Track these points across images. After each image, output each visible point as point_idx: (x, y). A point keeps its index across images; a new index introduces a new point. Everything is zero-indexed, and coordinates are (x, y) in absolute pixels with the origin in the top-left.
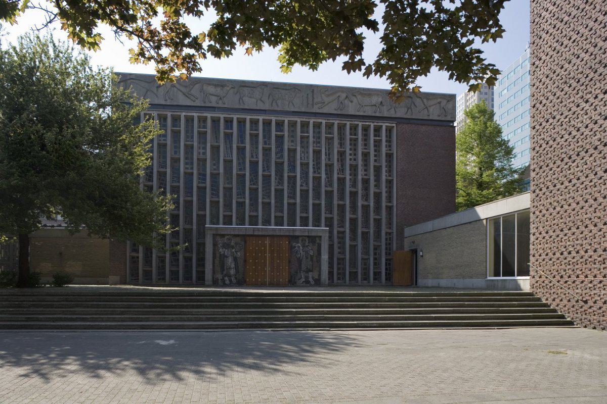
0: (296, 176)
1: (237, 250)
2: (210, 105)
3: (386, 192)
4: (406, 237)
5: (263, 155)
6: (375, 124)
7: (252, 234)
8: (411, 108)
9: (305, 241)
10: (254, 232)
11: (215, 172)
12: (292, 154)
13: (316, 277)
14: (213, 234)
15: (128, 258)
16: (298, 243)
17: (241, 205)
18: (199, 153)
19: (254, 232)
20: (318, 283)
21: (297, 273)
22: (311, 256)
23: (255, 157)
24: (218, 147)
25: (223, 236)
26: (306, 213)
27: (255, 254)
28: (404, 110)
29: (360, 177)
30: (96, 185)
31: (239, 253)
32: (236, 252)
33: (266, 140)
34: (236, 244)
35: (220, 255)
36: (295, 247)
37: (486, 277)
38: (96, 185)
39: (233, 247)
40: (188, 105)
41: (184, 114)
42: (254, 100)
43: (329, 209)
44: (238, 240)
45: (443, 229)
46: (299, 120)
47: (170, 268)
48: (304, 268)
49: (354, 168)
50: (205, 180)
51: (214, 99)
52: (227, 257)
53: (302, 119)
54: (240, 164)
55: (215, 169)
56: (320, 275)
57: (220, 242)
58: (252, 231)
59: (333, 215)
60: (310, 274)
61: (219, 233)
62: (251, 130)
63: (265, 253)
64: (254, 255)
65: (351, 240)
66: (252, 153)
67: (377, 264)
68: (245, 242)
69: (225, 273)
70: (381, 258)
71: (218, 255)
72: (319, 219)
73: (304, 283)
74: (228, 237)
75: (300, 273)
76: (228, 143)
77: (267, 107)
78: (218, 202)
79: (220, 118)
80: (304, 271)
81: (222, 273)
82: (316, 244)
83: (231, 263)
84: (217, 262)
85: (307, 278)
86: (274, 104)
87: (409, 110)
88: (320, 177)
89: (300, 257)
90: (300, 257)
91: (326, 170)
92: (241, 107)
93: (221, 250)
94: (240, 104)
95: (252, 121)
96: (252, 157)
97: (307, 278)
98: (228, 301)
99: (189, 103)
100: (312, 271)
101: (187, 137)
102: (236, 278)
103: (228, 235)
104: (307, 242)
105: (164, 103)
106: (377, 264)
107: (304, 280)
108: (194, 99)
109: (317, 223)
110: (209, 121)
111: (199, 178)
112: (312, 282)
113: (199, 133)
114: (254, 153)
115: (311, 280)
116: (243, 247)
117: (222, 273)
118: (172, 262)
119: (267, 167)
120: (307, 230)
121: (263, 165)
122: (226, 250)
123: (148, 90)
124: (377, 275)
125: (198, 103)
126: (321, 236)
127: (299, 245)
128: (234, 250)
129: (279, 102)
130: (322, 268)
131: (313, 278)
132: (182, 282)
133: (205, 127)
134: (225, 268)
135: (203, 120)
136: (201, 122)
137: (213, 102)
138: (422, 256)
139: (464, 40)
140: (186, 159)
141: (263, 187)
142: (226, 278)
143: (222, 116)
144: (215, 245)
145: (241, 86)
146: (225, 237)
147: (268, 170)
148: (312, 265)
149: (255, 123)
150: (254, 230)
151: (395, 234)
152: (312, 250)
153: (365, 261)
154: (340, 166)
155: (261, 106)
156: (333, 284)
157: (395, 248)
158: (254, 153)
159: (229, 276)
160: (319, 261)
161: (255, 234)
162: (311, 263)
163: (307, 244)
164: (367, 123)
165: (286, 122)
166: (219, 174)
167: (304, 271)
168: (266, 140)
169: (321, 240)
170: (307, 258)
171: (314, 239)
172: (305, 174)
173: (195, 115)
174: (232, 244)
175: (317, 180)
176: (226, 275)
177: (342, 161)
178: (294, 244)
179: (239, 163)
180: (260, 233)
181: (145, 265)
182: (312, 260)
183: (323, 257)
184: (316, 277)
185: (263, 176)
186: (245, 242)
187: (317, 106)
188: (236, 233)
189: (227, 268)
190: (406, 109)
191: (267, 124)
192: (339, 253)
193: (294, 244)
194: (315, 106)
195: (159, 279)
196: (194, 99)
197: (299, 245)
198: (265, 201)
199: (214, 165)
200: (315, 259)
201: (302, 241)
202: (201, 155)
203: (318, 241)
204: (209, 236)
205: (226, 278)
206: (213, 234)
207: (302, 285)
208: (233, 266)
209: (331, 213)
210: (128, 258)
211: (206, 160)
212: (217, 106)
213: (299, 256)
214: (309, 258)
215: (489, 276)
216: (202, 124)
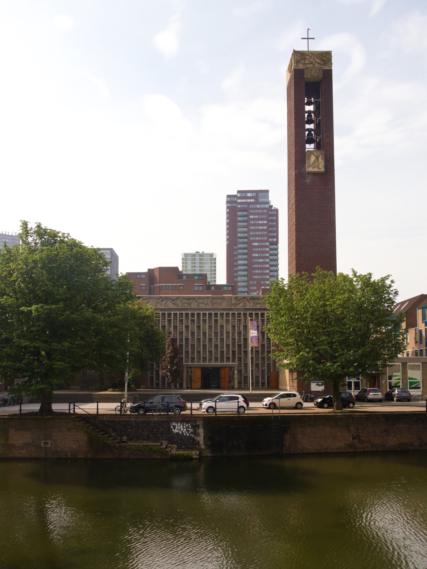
0: (224, 338)
5: (209, 329)
6: (261, 312)
11: (187, 337)
12: (221, 328)
15: (149, 377)
17: (199, 352)
18: (180, 329)
24: (188, 326)
25: (191, 368)
41: (173, 312)
43: (240, 353)
50: (182, 341)
51: (186, 305)
53: (226, 312)
55: (187, 336)
62: (180, 317)
67: (263, 378)
70: (265, 376)
71: (189, 376)
77: (210, 307)
78: (188, 351)
79: (183, 313)
84: (188, 379)
86: (213, 306)
88: (235, 338)
91: (238, 335)
92: (198, 308)
93: (190, 374)
95: (227, 314)
96: (204, 329)
99: (175, 307)
101: (174, 322)
105: (164, 308)
108: (177, 305)
109: (233, 361)
110: (184, 315)
111: (180, 340)
113: (180, 320)
121: (209, 333)
123: (157, 303)
124: (263, 384)
125: (180, 307)
129: (216, 305)
133: (182, 317)
135: (233, 314)
137: (186, 306)
139: (405, 355)
141: (209, 344)
143: (178, 312)
144: (187, 372)
145: (198, 299)
149: (187, 315)
151: (272, 364)
155: (207, 307)
165: (236, 314)
166: (189, 338)
171: (231, 368)
172: (228, 337)
173: (178, 312)
175: (234, 339)
177: (246, 330)
179: (198, 333)
183: (235, 376)
184: (232, 385)
185: (209, 338)
187: (233, 306)
192: (262, 341)
194: (232, 306)
196: (177, 305)
200: (232, 377)
202: (181, 330)
203: (233, 369)
210: (149, 377)
211: (183, 332)
212: (187, 308)
216: (181, 316)
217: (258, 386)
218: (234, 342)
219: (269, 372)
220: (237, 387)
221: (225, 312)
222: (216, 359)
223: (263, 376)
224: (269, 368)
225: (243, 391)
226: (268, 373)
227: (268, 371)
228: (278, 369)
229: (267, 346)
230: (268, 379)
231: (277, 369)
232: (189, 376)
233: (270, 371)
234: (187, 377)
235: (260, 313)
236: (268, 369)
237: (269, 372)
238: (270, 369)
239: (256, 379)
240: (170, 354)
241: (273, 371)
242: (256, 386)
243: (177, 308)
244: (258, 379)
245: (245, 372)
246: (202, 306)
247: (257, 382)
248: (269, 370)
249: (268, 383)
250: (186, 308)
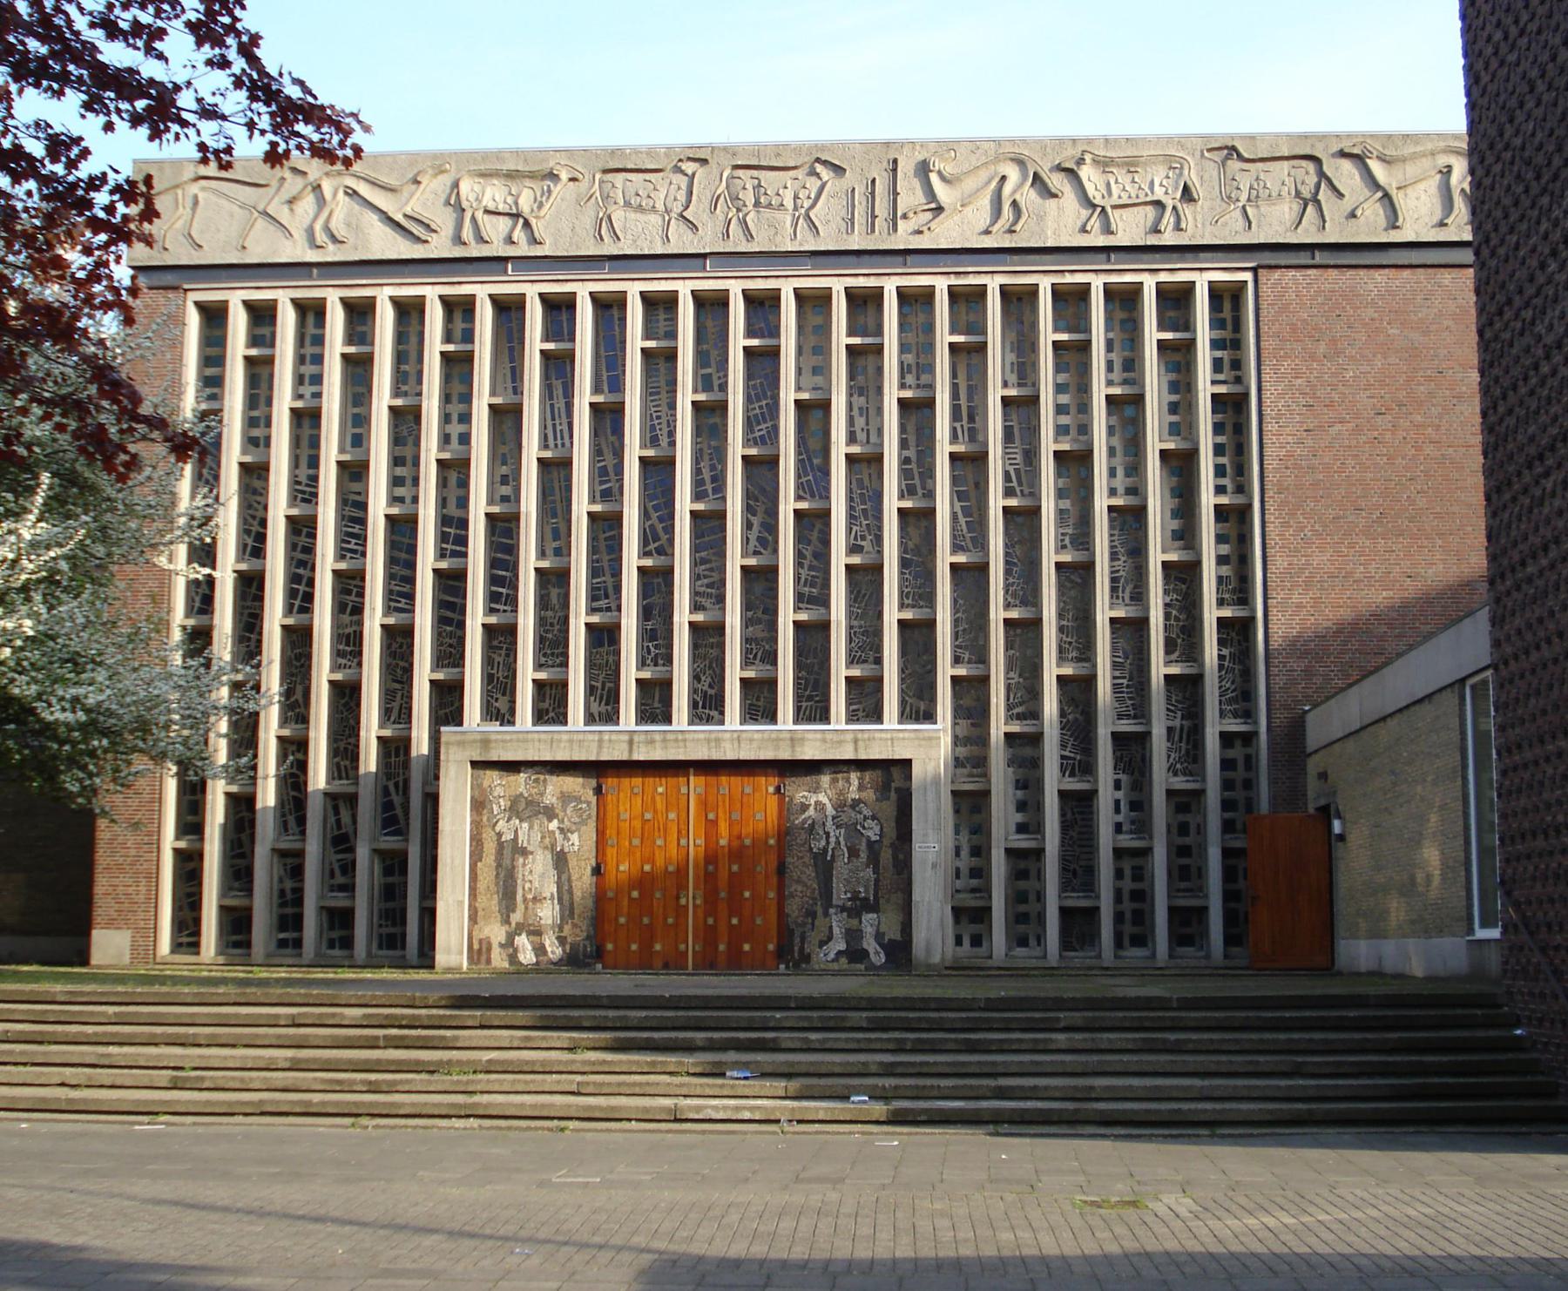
2: (485, 251)
3: (1221, 560)
4: (1316, 752)
6: (1164, 277)
7: (625, 757)
8: (1318, 203)
10: (631, 751)
13: (893, 933)
16: (816, 789)
19: (631, 751)
20: (673, 964)
21: (813, 915)
22: (870, 844)
23: (664, 441)
28: (1286, 210)
29: (1101, 503)
31: (574, 838)
32: (561, 830)
33: (709, 371)
34: (565, 798)
35: (501, 846)
36: (805, 807)
37: (1471, 931)
39: (550, 813)
40: (831, 248)
42: (655, 220)
44: (572, 783)
45: (1377, 722)
46: (431, 293)
47: (321, 897)
48: (840, 895)
49: (1075, 463)
52: (524, 852)
54: (607, 474)
56: (907, 927)
57: (499, 791)
58: (625, 746)
60: (869, 919)
65: (1068, 767)
66: (653, 428)
70: (1203, 848)
71: (490, 847)
73: (843, 960)
75: (826, 914)
76: (560, 391)
77: (707, 241)
80: (843, 909)
81: (507, 921)
85: (853, 935)
87: (1310, 209)
89: (825, 850)
90: (825, 850)
93: (501, 826)
94: (602, 239)
95: (648, 300)
97: (853, 935)
98: (381, 1043)
99: (403, 249)
100: (874, 908)
102: (562, 940)
105: (312, 256)
106: (1186, 870)
107: (842, 946)
112: (878, 958)
114: (659, 429)
115: (870, 945)
117: (507, 921)
118: (332, 875)
119: (714, 479)
122: (525, 825)
125: (439, 247)
126: (909, 761)
127: (823, 798)
128: (554, 825)
130: (916, 897)
131: (879, 936)
132: (363, 955)
134: (519, 897)
135: (916, 302)
136: (458, 316)
138: (1341, 838)
140: (396, 465)
142: (522, 941)
144: (479, 805)
147: (715, 490)
148: (877, 881)
150: (631, 742)
151: (1263, 736)
152: (874, 818)
153: (1132, 860)
154: (1019, 458)
155: (681, 242)
157: (1264, 806)
158: (659, 429)
159: (536, 932)
160: (903, 865)
161: (637, 757)
164: (1128, 278)
167: (843, 909)
168: (709, 371)
170: (854, 853)
174: (550, 798)
176: (520, 928)
181: (231, 889)
182: (874, 859)
184: (893, 933)
189: (525, 900)
190: (1296, 206)
191: (711, 306)
192: (1022, 828)
195: (331, 945)
199: (504, 480)
205: (522, 941)
207: (835, 966)
214: (863, 855)
215: (1483, 925)
216: (459, 325)
217: (1140, 940)
218: (917, 550)
219: (1238, 816)
220: (928, 610)
221: (838, 286)
222: (760, 702)
223: (1184, 851)
224: (1240, 774)
225: (1264, 1145)
226: (1228, 827)
227: (1227, 805)
228: (1323, 776)
229: (1220, 579)
230: (1229, 874)
231: (1312, 785)
232: (490, 847)
233: (1250, 806)
234: (476, 855)
235: (1149, 283)
236: (1227, 785)
237: (1238, 816)
238: (1248, 784)
239: (1119, 874)
240: (78, 516)
241: (1273, 799)
242: (1119, 944)
243: (418, 252)
244: (1139, 874)
245: (1019, 817)
246: (639, 235)
247: (1127, 906)
248: (1239, 794)
249: (1230, 918)
250: (497, 249)
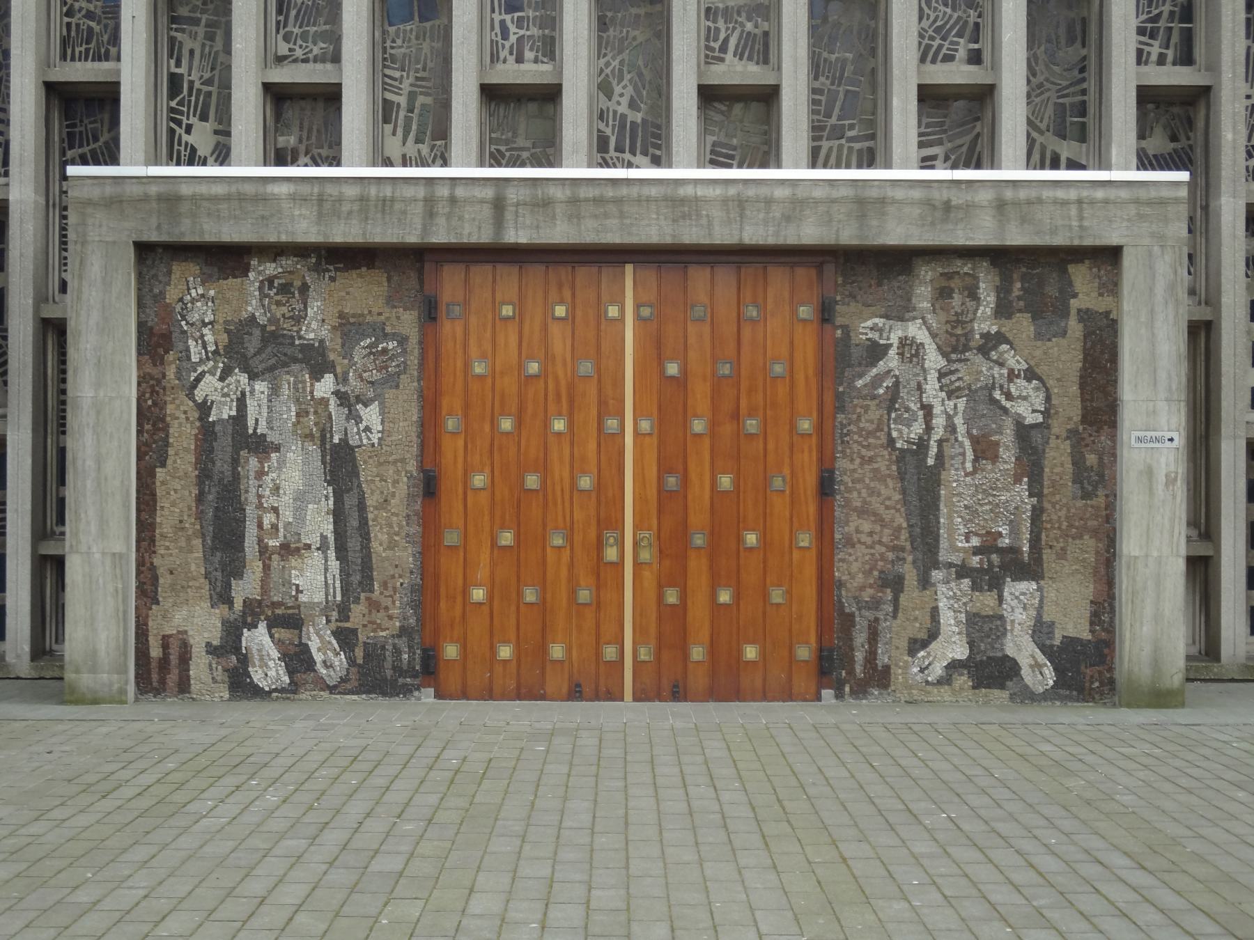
1: (354, 385)
9: (973, 294)
14: (144, 250)
16: (902, 313)
21: (897, 584)
22: (1023, 432)
26: (975, 58)
27: (519, 423)
30: (889, 498)
32: (342, 397)
34: (349, 328)
35: (207, 432)
36: (876, 352)
38: (889, 498)
39: (316, 361)
52: (261, 446)
59: (1213, 67)
61: (188, 232)
63: (609, 405)
64: (506, 424)
68: (430, 312)
69: (246, 588)
71: (183, 434)
72: (1082, 110)
74: (270, 269)
75: (925, 583)
80: (962, 571)
81: (223, 597)
82: (1074, 327)
83: (301, 499)
89: (922, 444)
90: (922, 444)
93: (209, 387)
102: (345, 638)
103: (275, 251)
104: (988, 298)
107: (960, 651)
112: (1040, 675)
116: (413, 360)
120: (985, 196)
122: (261, 386)
126: (1112, 255)
127: (915, 330)
128: (325, 387)
131: (1041, 630)
142: (259, 639)
146: (245, 271)
148: (1037, 513)
152: (1030, 375)
156: (1216, 669)
162: (1020, 494)
163: (984, 322)
169: (1112, 287)
170: (985, 450)
176: (252, 613)
178: (867, 327)
180: (560, 233)
186: (430, 312)
188: (344, 233)
189: (263, 550)
193: (867, 327)
197: (915, 330)
198: (509, 73)
200: (1058, 458)
201: (943, 294)
204: (95, 267)
205: (259, 639)
206: (144, 250)
208: (319, 524)
209: (1186, 58)
213: (918, 428)
214: (1008, 455)
